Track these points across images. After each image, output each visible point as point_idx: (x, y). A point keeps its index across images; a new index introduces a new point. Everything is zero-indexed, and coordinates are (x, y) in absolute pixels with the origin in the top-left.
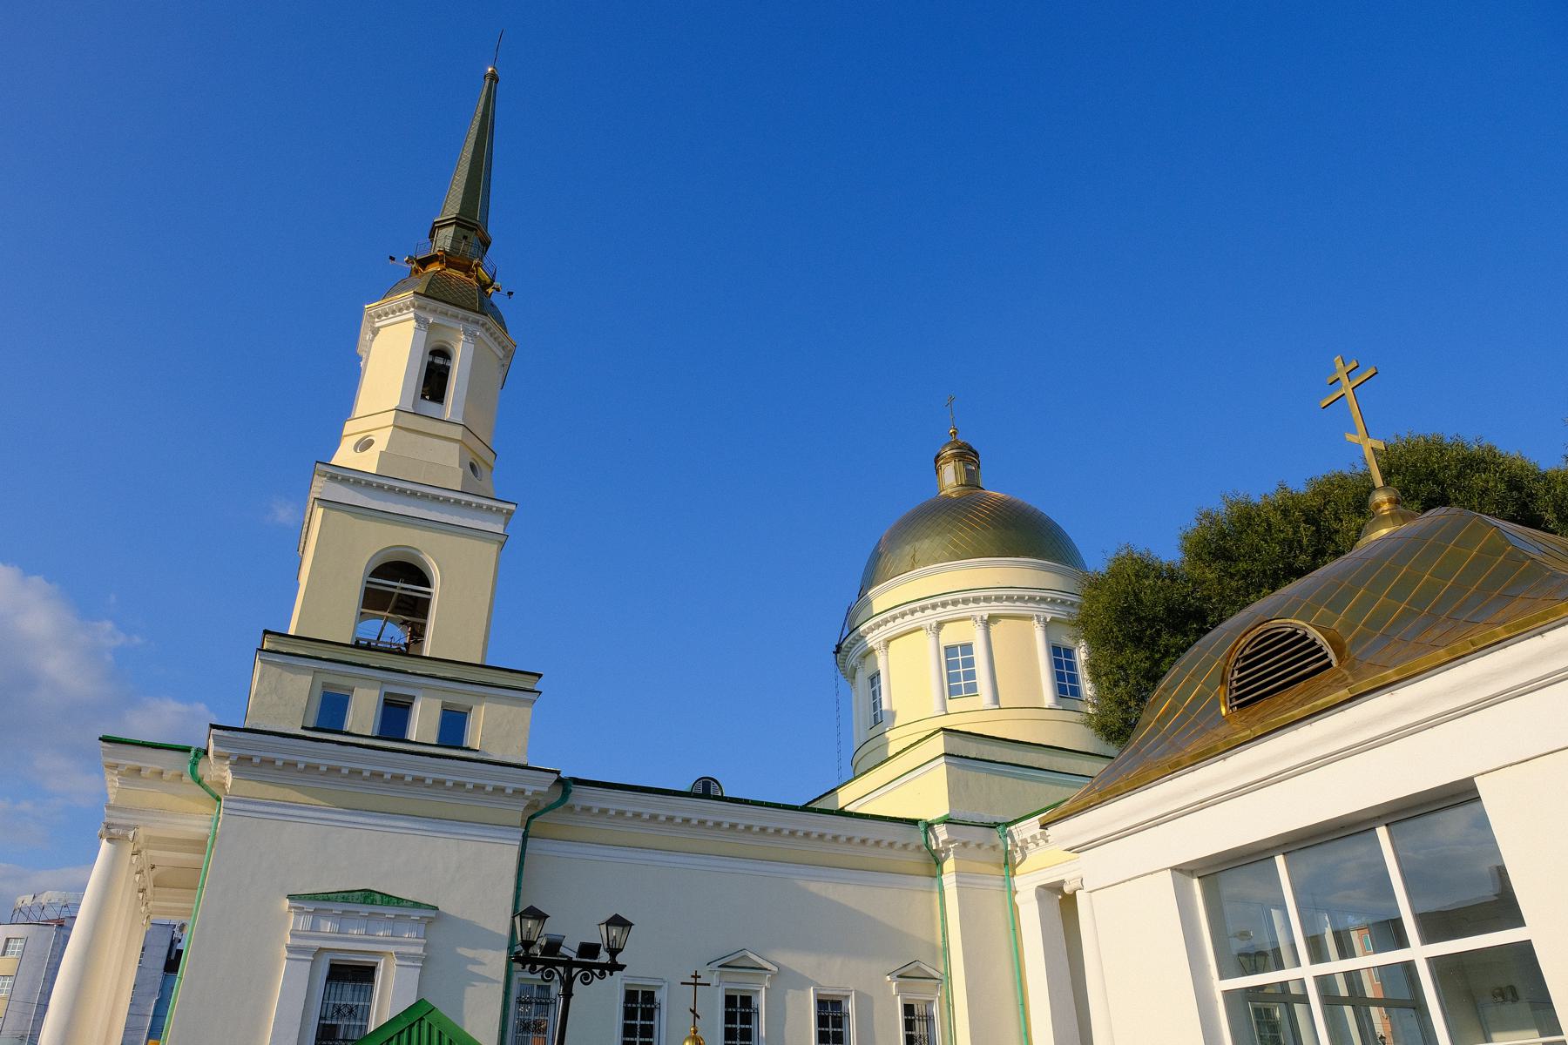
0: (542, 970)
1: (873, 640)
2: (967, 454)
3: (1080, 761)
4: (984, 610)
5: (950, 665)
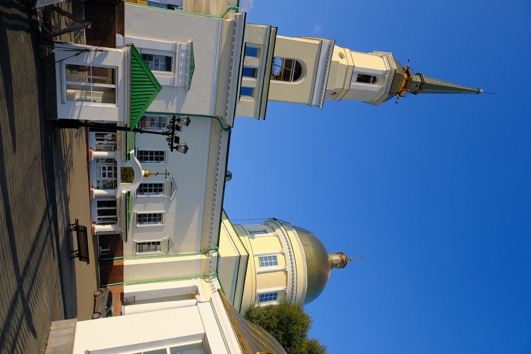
0: (171, 125)
1: (278, 231)
2: (343, 264)
4: (289, 269)
5: (270, 257)
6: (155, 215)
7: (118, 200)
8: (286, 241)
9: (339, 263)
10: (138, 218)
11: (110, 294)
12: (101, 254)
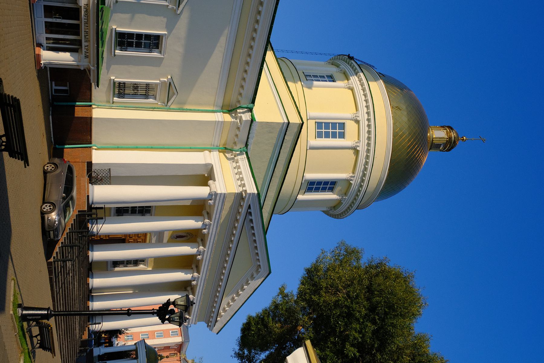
1: (354, 80)
2: (450, 145)
3: (275, 192)
4: (362, 149)
5: (334, 125)
6: (148, 37)
7: (82, 8)
8: (364, 100)
9: (443, 143)
10: (118, 39)
11: (70, 170)
12: (53, 94)
